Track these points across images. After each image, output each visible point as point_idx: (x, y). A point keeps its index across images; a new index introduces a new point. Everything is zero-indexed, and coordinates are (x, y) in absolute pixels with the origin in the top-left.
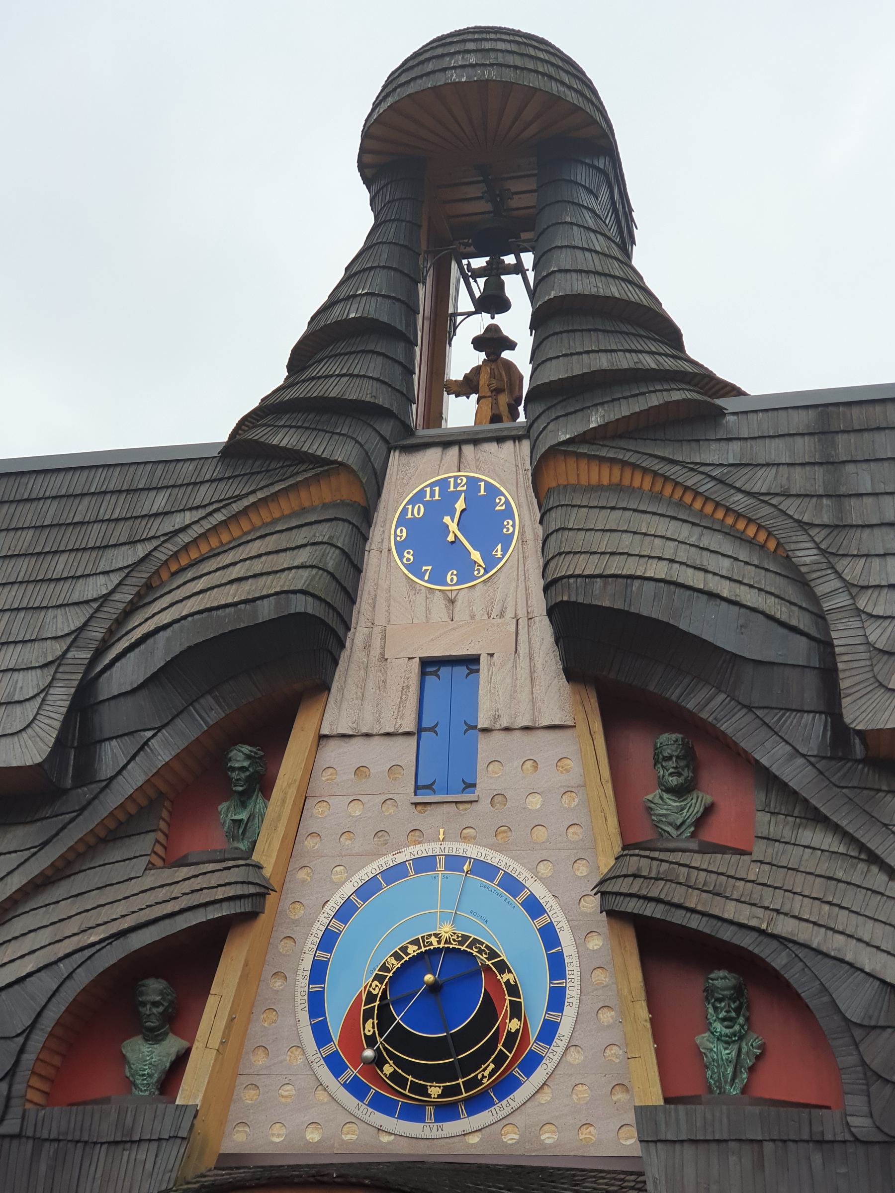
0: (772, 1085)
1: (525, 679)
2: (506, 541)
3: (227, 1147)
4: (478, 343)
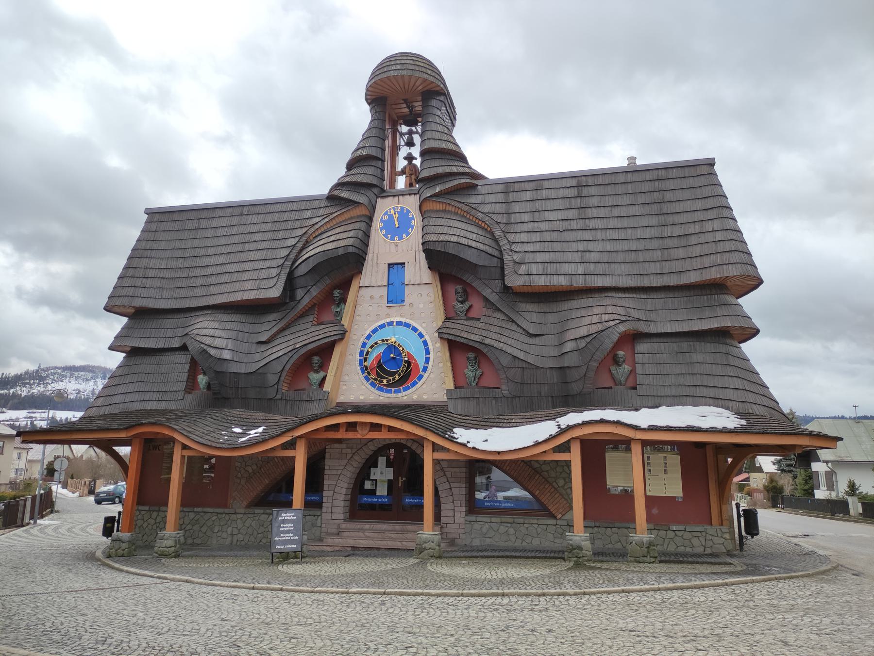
0: (485, 382)
1: (418, 271)
2: (412, 227)
3: (338, 401)
4: (405, 158)
